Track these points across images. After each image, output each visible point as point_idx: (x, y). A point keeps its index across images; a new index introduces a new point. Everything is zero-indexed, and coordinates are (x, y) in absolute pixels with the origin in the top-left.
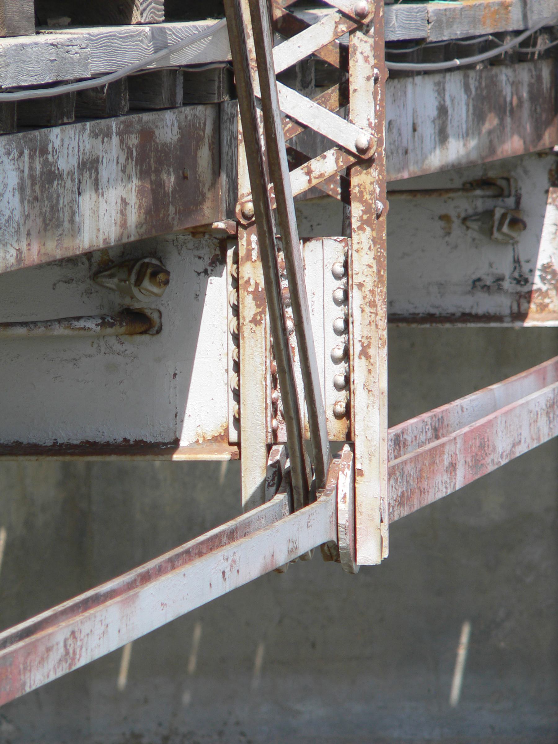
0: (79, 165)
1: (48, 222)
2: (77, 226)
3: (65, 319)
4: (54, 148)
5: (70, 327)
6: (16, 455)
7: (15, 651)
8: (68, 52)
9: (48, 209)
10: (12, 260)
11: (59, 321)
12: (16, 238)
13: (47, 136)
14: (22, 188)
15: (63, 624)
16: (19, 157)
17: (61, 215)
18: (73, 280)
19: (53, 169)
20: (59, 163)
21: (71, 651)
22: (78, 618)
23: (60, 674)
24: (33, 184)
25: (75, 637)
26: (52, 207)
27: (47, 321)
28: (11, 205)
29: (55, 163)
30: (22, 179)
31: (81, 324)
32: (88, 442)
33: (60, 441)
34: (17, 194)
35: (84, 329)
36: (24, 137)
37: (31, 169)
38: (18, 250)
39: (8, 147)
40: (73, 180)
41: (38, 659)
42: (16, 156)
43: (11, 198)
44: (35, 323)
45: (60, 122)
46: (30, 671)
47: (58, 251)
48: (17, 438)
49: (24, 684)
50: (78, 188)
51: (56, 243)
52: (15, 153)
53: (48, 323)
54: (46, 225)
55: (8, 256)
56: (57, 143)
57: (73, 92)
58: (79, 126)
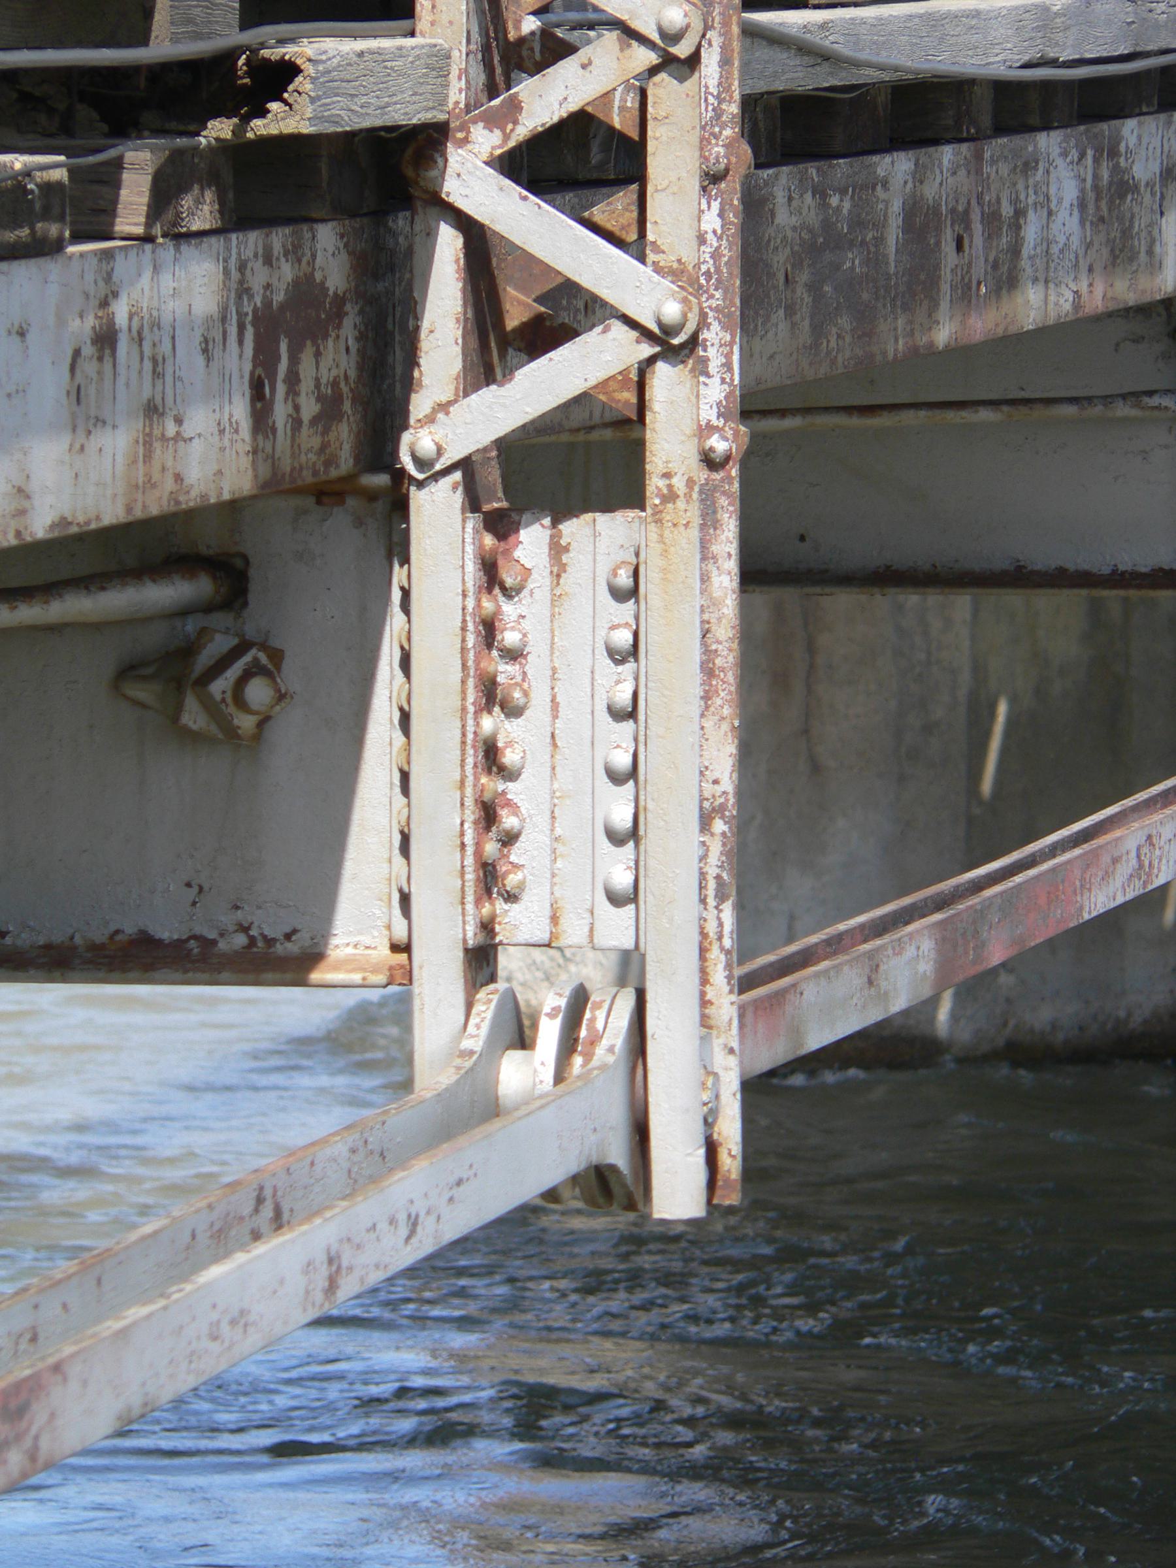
0: (1161, 172)
1: (1117, 252)
2: (1157, 258)
3: (1133, 394)
4: (1127, 147)
5: (1138, 405)
6: (1059, 586)
7: (1069, 862)
8: (1150, 11)
9: (1118, 235)
10: (1068, 307)
11: (1124, 397)
12: (1073, 276)
13: (1119, 131)
14: (1082, 205)
15: (1136, 825)
16: (1080, 160)
17: (1136, 243)
18: (1143, 338)
19: (1126, 177)
20: (1135, 169)
21: (1147, 863)
22: (1156, 817)
23: (1130, 895)
24: (1098, 199)
25: (1152, 844)
26: (1124, 232)
27: (1107, 396)
28: (1066, 228)
29: (1128, 170)
30: (1083, 191)
31: (1155, 401)
32: (1161, 569)
33: (1121, 568)
34: (1076, 212)
35: (1158, 408)
36: (1087, 131)
37: (1096, 176)
38: (1076, 292)
39: (1064, 145)
40: (1153, 194)
41: (1100, 874)
42: (1076, 159)
43: (1068, 217)
44: (1089, 399)
45: (1137, 111)
46: (1090, 890)
47: (1131, 295)
48: (1060, 563)
49: (1081, 908)
50: (1160, 206)
51: (1128, 283)
52: (1074, 154)
53: (1108, 400)
54: (1115, 257)
55: (1062, 301)
56: (1132, 141)
57: (1156, 69)
58: (1163, 117)
